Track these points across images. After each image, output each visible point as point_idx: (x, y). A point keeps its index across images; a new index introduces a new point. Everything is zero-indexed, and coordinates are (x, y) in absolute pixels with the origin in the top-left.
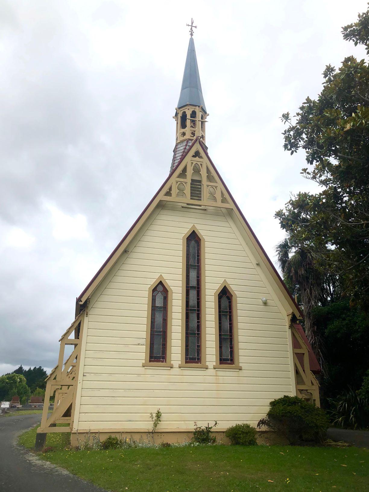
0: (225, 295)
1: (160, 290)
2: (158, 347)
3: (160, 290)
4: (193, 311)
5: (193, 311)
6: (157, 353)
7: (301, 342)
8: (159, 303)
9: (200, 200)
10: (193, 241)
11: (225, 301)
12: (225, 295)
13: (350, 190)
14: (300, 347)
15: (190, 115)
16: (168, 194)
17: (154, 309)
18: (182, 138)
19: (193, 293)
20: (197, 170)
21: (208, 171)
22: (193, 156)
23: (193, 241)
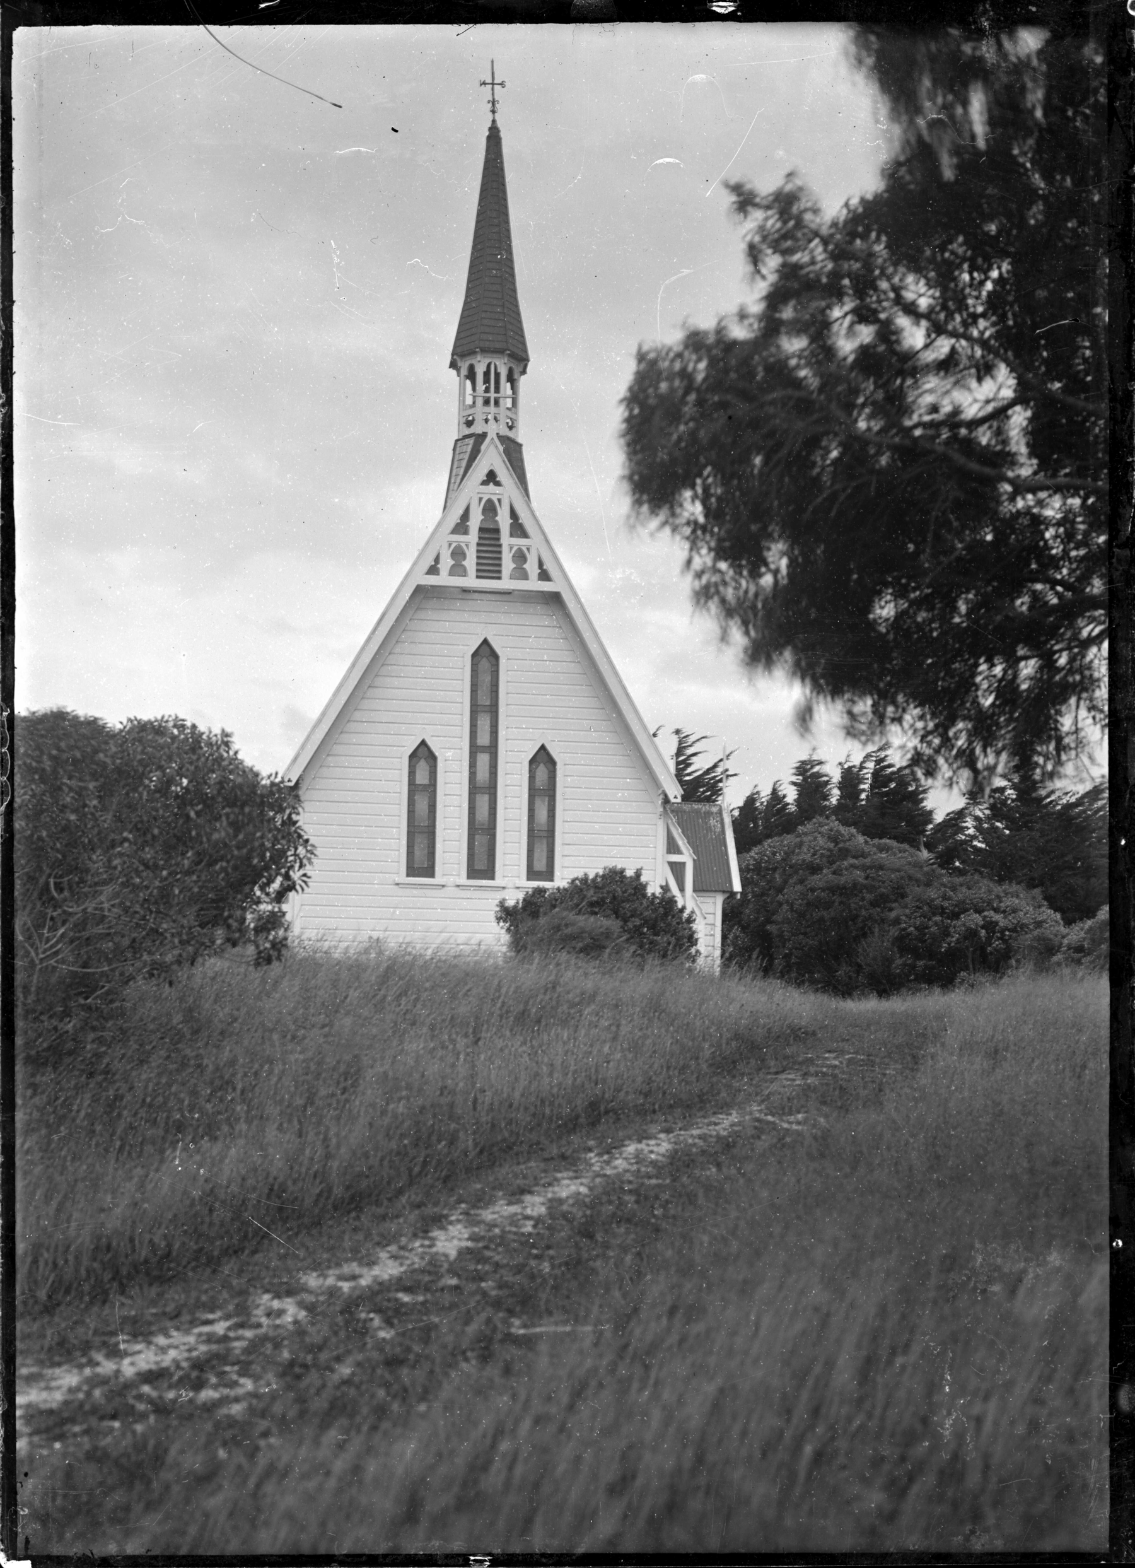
0: (543, 759)
1: (423, 755)
2: (420, 853)
3: (423, 755)
4: (483, 789)
5: (483, 789)
6: (421, 863)
7: (681, 842)
8: (422, 778)
9: (499, 578)
10: (485, 656)
11: (542, 772)
12: (543, 759)
13: (908, 584)
14: (678, 851)
15: (494, 138)
16: (433, 570)
17: (413, 788)
18: (468, 431)
19: (483, 759)
20: (490, 509)
21: (514, 515)
22: (484, 483)
23: (485, 656)
